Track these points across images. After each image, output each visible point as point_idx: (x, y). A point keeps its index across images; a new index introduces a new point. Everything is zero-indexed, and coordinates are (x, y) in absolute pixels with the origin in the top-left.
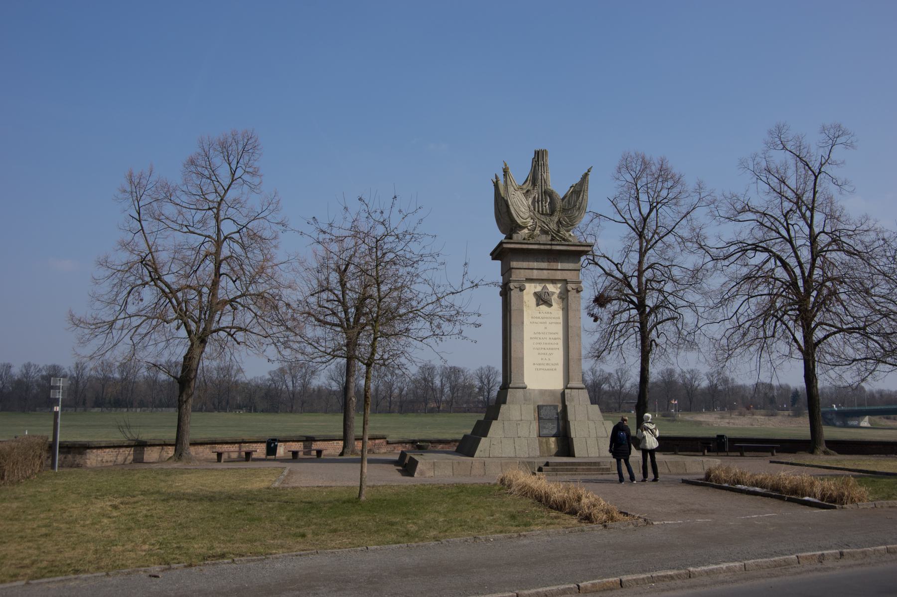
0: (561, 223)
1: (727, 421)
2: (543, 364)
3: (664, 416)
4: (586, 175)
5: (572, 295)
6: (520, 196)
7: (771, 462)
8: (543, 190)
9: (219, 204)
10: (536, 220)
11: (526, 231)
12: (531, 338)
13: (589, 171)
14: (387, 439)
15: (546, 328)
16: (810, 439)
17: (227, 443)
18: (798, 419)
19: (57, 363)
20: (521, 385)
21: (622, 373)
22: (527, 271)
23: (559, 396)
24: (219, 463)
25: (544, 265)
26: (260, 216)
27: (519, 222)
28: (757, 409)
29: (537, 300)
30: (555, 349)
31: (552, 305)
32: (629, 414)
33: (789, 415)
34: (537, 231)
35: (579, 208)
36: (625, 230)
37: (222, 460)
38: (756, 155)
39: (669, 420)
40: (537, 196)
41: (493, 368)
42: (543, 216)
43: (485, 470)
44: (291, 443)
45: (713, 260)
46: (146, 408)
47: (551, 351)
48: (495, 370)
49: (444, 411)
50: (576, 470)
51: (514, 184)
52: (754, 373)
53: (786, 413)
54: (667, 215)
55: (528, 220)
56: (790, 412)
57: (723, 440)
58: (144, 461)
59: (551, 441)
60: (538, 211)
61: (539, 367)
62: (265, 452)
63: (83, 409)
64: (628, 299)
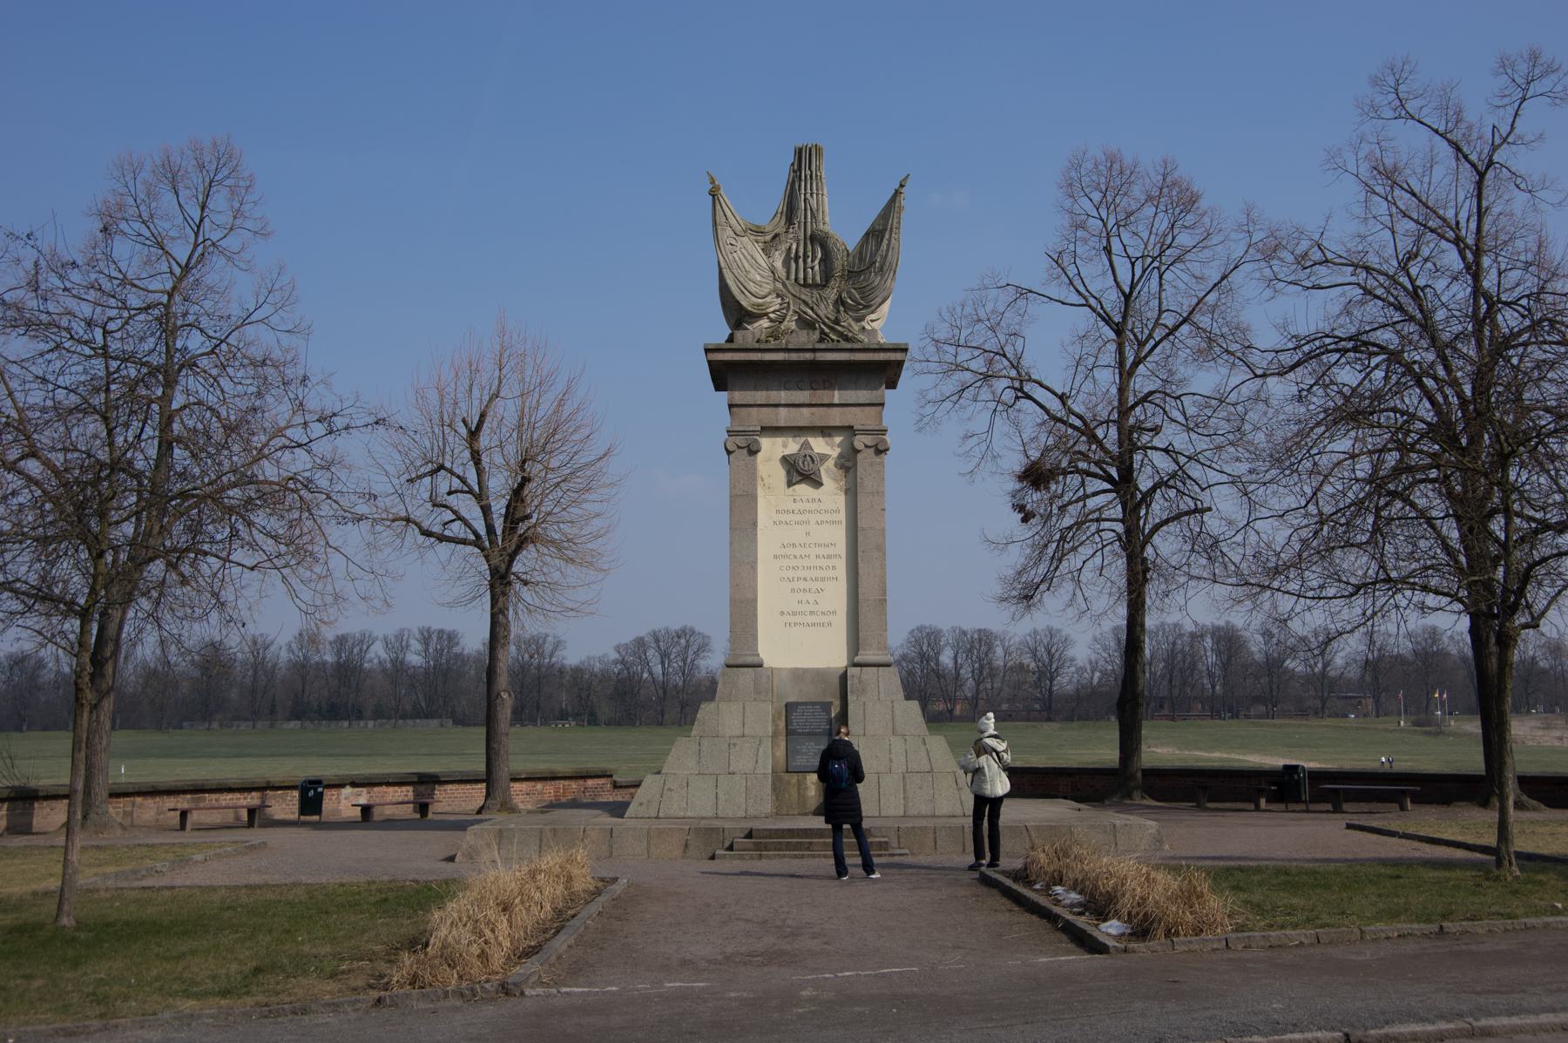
0: (843, 303)
2: (802, 613)
3: (1417, 724)
5: (865, 459)
6: (750, 246)
7: (1349, 827)
8: (809, 233)
9: (170, 295)
10: (789, 299)
11: (765, 323)
13: (902, 186)
14: (615, 778)
15: (808, 534)
16: (1484, 773)
17: (230, 790)
20: (750, 660)
22: (764, 410)
23: (836, 682)
24: (182, 833)
26: (254, 318)
27: (744, 303)
29: (788, 473)
30: (829, 579)
32: (1343, 720)
34: (790, 323)
35: (881, 269)
37: (189, 826)
40: (794, 247)
41: (1059, 631)
43: (611, 846)
44: (384, 788)
45: (1256, 376)
46: (384, 721)
47: (819, 585)
48: (1063, 634)
49: (961, 719)
50: (809, 847)
51: (733, 221)
54: (1179, 288)
55: (768, 299)
57: (1296, 777)
58: (34, 831)
59: (809, 783)
60: (796, 280)
61: (793, 619)
62: (296, 808)
63: (268, 723)
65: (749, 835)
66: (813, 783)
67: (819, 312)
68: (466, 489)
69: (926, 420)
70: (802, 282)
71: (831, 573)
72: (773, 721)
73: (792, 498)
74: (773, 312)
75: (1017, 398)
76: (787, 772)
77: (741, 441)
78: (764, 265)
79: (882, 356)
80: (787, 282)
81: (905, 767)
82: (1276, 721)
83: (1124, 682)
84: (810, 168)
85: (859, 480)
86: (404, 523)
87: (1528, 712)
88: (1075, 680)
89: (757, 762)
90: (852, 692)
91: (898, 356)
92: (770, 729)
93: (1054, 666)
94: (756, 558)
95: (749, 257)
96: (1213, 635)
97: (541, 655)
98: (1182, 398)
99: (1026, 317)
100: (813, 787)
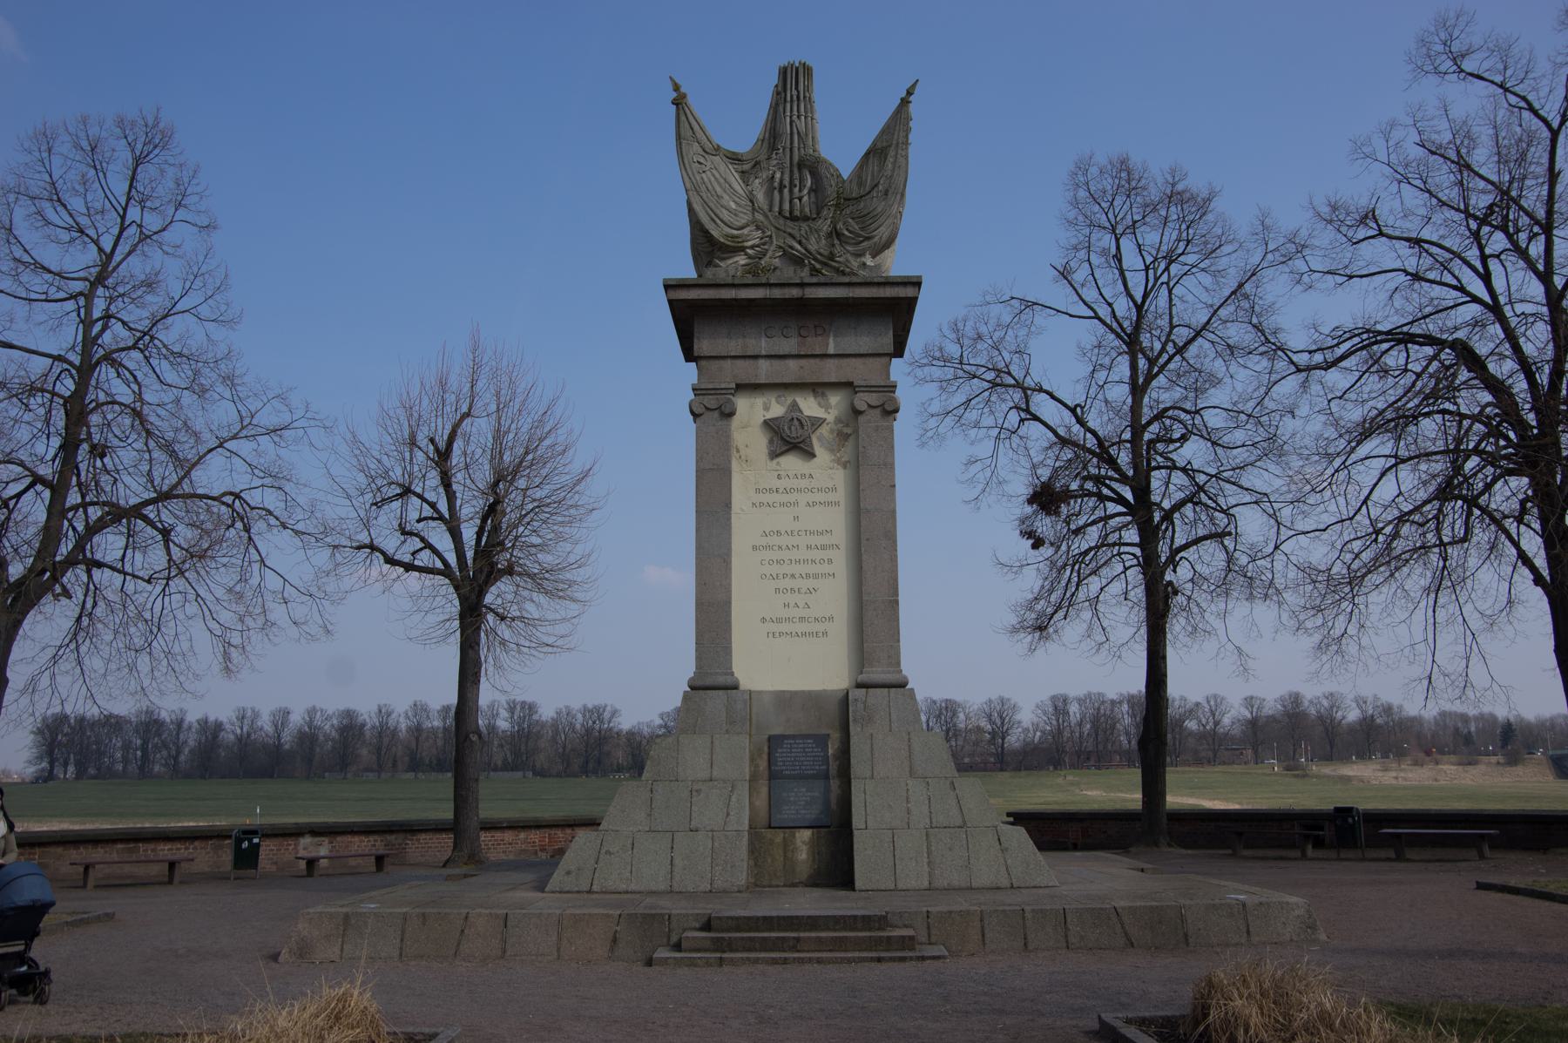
0: (839, 235)
1: (1394, 774)
3: (1288, 769)
4: (905, 102)
7: (1481, 886)
11: (741, 260)
12: (755, 548)
15: (796, 518)
18: (1514, 768)
19: (352, 706)
20: (721, 680)
21: (1216, 701)
22: (739, 362)
25: (789, 345)
26: (179, 307)
27: (715, 233)
28: (1443, 753)
30: (824, 575)
31: (813, 455)
33: (1498, 763)
34: (773, 259)
36: (1089, 332)
38: (1393, 125)
39: (1296, 776)
40: (778, 175)
41: (1009, 700)
42: (789, 223)
44: (349, 838)
47: (811, 583)
48: (1012, 702)
50: (795, 945)
52: (1421, 648)
53: (1494, 759)
55: (745, 231)
56: (1501, 758)
57: (1350, 820)
59: (798, 842)
64: (1105, 491)
65: (707, 926)
66: (803, 842)
67: (810, 247)
68: (435, 515)
69: (930, 434)
70: (787, 215)
71: (826, 568)
72: (752, 760)
73: (776, 474)
74: (752, 247)
75: (1022, 420)
76: (770, 827)
77: (711, 401)
78: (741, 192)
79: (889, 292)
80: (769, 214)
81: (928, 821)
82: (1179, 769)
83: (1146, 720)
84: (797, 88)
85: (861, 449)
86: (369, 551)
87: (1370, 758)
88: (1021, 738)
89: (728, 814)
90: (854, 720)
91: (908, 292)
92: (747, 770)
93: (1005, 728)
94: (730, 549)
95: (722, 181)
96: (1129, 702)
97: (602, 722)
98: (1202, 412)
99: (1033, 329)
100: (804, 847)
